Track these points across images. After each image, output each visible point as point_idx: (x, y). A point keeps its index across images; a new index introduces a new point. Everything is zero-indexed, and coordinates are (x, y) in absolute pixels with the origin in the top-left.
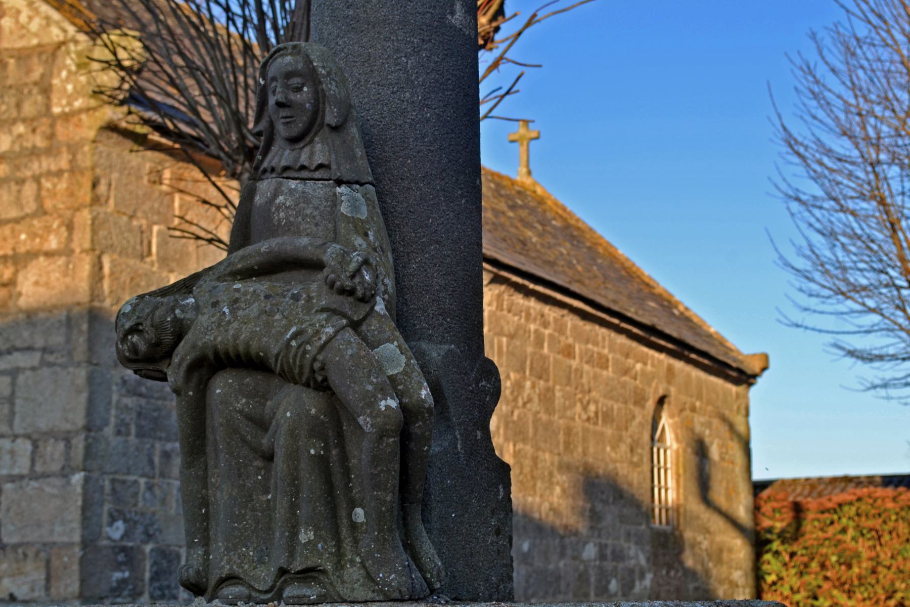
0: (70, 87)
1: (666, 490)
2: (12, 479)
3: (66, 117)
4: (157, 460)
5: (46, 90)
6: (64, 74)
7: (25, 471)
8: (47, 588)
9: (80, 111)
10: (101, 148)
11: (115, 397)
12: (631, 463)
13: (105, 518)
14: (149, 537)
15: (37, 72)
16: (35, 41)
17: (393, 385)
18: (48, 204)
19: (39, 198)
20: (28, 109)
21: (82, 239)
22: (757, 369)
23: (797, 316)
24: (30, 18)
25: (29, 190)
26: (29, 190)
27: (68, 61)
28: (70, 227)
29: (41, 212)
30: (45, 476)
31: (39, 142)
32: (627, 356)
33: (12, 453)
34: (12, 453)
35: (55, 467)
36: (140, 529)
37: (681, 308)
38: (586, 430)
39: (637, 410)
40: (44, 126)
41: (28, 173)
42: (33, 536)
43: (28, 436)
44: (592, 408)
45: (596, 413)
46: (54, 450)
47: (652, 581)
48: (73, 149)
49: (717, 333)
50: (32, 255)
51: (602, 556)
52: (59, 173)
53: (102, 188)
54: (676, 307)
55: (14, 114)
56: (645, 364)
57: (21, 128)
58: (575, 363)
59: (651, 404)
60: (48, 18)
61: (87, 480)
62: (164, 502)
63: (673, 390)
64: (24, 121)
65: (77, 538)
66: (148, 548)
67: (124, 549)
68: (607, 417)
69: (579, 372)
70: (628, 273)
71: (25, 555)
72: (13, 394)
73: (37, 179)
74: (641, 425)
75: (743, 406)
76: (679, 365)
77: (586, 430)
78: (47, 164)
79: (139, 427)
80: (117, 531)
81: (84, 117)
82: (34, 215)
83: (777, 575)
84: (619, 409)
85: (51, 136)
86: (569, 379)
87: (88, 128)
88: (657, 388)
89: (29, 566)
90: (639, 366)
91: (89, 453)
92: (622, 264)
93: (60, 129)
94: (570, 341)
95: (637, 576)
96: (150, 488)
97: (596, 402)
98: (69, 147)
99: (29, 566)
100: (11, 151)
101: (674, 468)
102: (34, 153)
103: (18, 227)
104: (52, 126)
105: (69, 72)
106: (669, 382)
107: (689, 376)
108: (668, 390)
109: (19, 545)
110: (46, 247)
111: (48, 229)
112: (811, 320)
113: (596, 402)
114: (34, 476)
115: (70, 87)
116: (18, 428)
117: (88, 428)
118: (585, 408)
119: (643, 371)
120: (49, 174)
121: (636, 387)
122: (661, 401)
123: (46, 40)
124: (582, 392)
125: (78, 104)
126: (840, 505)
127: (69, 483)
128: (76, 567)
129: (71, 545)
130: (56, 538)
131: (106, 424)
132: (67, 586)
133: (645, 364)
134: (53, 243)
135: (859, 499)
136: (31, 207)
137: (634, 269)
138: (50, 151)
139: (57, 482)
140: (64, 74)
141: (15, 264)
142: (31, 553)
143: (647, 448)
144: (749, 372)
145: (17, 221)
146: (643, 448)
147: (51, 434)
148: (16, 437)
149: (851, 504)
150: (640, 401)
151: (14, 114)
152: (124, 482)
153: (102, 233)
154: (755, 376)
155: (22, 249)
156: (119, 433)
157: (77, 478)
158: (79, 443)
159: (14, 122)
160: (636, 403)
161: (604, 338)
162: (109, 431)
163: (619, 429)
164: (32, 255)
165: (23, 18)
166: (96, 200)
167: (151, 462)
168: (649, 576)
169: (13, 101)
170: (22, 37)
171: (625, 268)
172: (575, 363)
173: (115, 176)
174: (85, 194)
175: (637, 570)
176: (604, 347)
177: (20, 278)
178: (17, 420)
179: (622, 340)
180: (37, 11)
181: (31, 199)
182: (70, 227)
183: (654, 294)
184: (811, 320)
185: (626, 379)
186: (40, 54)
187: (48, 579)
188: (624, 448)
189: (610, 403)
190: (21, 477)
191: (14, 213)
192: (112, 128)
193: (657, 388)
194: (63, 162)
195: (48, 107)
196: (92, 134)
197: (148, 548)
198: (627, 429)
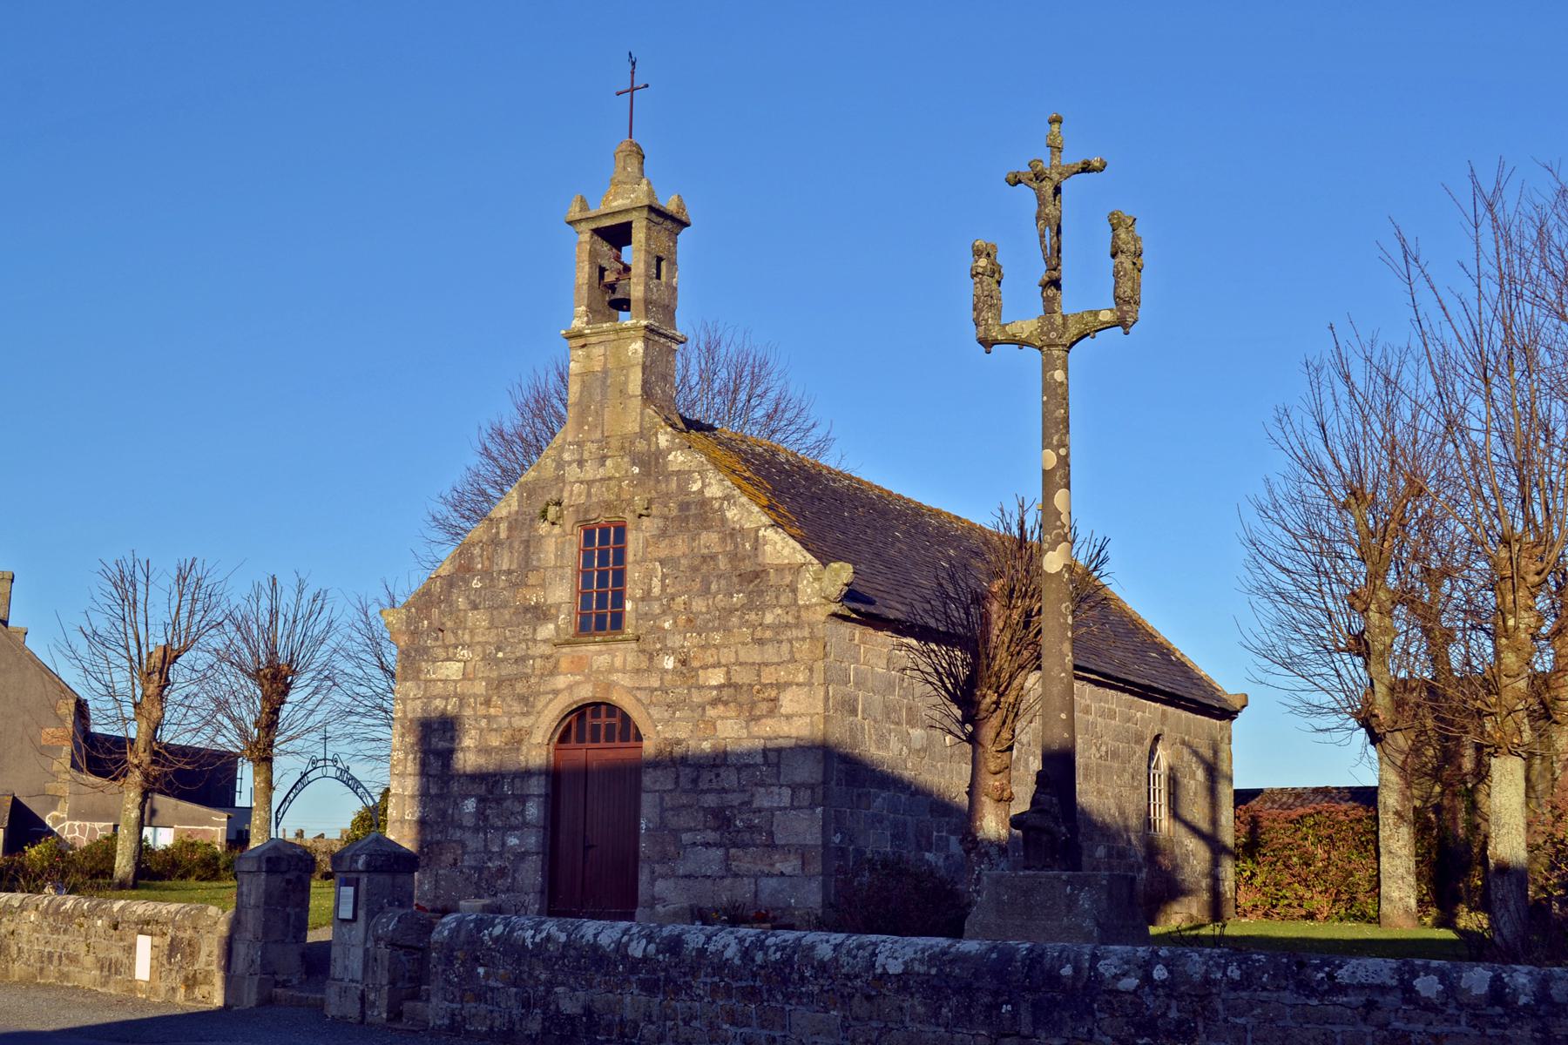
0: (809, 590)
1: (1160, 806)
2: (780, 809)
3: (807, 607)
4: (854, 798)
5: (794, 591)
6: (805, 582)
7: (788, 805)
8: (803, 869)
9: (816, 605)
10: (828, 625)
11: (836, 765)
12: (1132, 786)
13: (832, 832)
14: (852, 842)
15: (788, 579)
16: (786, 561)
17: (1064, 835)
18: (797, 656)
19: (791, 652)
20: (783, 600)
21: (818, 677)
22: (1238, 708)
23: (1261, 676)
24: (783, 547)
25: (785, 647)
26: (785, 647)
27: (808, 575)
28: (811, 670)
29: (793, 660)
30: (800, 808)
31: (791, 620)
32: (1130, 708)
33: (780, 794)
34: (780, 794)
35: (806, 803)
36: (848, 837)
37: (1178, 655)
38: (1099, 765)
39: (1137, 748)
40: (793, 610)
41: (785, 638)
42: (794, 840)
43: (789, 786)
44: (1104, 748)
45: (1107, 752)
46: (805, 795)
47: (1147, 873)
48: (811, 625)
49: (1206, 676)
50: (788, 684)
51: (1109, 855)
52: (804, 639)
53: (828, 648)
54: (1174, 654)
55: (775, 602)
56: (1144, 712)
57: (779, 611)
58: (1091, 718)
59: (1148, 743)
60: (794, 548)
61: (824, 811)
62: (858, 822)
63: (1165, 729)
64: (781, 607)
65: (820, 843)
66: (851, 848)
67: (841, 848)
68: (1115, 754)
69: (1094, 724)
70: (1134, 625)
71: (789, 851)
72: (779, 761)
73: (790, 642)
74: (1141, 758)
75: (1227, 735)
76: (1170, 709)
77: (1099, 765)
78: (795, 633)
79: (846, 781)
80: (837, 839)
81: (818, 608)
82: (789, 662)
83: (1251, 872)
84: (1123, 748)
85: (798, 617)
86: (1087, 730)
87: (820, 614)
88: (1153, 729)
89: (792, 857)
90: (1139, 714)
91: (825, 797)
92: (1131, 616)
93: (803, 614)
94: (1088, 702)
95: (180, 872)
96: (851, 814)
97: (1107, 744)
98: (809, 624)
99: (792, 857)
100: (773, 623)
101: (1167, 788)
102: (787, 625)
103: (779, 668)
104: (798, 611)
105: (808, 581)
106: (1163, 724)
107: (1179, 717)
108: (1162, 730)
109: (786, 846)
110: (796, 680)
111: (798, 670)
112: (1271, 679)
113: (1107, 744)
114: (793, 807)
115: (809, 590)
116: (782, 780)
117: (824, 783)
118: (1098, 750)
119: (1142, 717)
120: (797, 639)
121: (1137, 730)
122: (1157, 738)
123: (793, 561)
124: (1097, 738)
125: (814, 600)
126: (1302, 817)
127: (814, 812)
128: (820, 858)
129: (816, 846)
130: (807, 842)
131: (832, 780)
132: (814, 868)
133: (1144, 712)
134: (801, 678)
135: (1319, 813)
136: (786, 657)
137: (1140, 621)
138: (797, 626)
139: (809, 812)
140: (805, 582)
141: (778, 688)
142: (793, 851)
143: (1145, 775)
144: (1231, 709)
145: (778, 664)
146: (1141, 776)
147: (803, 785)
148: (781, 786)
149: (1311, 815)
150: (1139, 740)
151: (775, 602)
152: (840, 811)
153: (829, 673)
154: (1236, 712)
155: (782, 681)
156: (838, 784)
157: (819, 810)
158: (820, 791)
159: (775, 606)
160: (1136, 742)
161: (1112, 696)
162: (833, 783)
163: (1123, 762)
164: (788, 684)
165: (779, 547)
166: (826, 655)
167: (852, 800)
168: (1145, 870)
169: (774, 594)
170: (779, 558)
171: (1132, 620)
172: (1091, 718)
173: (834, 639)
174: (819, 652)
175: (1136, 866)
176: (1112, 704)
177: (781, 697)
178: (782, 777)
179: (1126, 696)
180: (787, 545)
181: (787, 652)
182: (811, 670)
183: (1156, 643)
184: (1271, 679)
185: (1129, 724)
186: (790, 569)
187: (803, 864)
188: (1127, 776)
189: (1117, 744)
190: (786, 808)
191: (776, 660)
192: (835, 615)
193: (1153, 729)
194: (806, 633)
195: (796, 600)
196: (823, 618)
197: (851, 848)
198: (1129, 762)
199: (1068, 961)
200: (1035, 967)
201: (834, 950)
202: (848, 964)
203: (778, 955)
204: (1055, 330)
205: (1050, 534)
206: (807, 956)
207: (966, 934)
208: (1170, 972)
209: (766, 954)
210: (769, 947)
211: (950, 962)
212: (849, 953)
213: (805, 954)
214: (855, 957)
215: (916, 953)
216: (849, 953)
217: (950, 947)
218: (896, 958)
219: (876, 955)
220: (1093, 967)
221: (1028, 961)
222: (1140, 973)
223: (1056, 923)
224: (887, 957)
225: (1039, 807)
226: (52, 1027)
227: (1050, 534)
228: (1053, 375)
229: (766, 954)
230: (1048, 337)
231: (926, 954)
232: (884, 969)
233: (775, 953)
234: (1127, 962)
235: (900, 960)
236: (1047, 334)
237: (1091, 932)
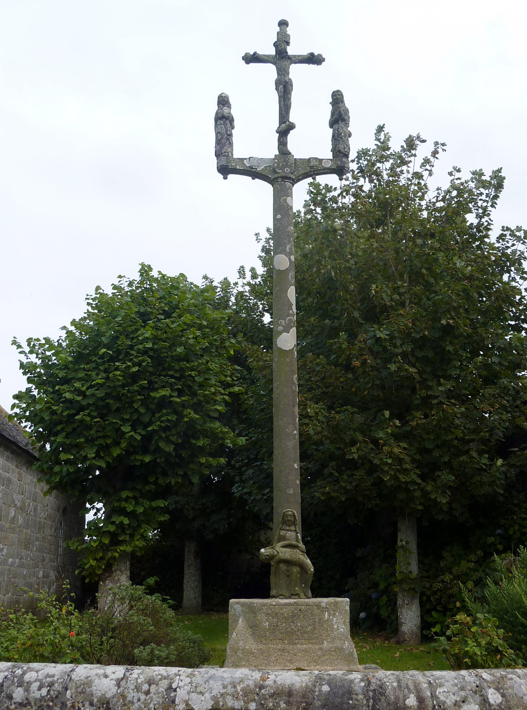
199: (410, 692)
200: (380, 700)
201: (118, 685)
202: (139, 700)
203: (44, 691)
204: (289, 167)
205: (285, 319)
206: (82, 692)
207: (229, 661)
208: (503, 695)
209: (27, 690)
210: (29, 683)
211: (272, 695)
212: (138, 688)
213: (79, 690)
214: (147, 693)
215: (225, 687)
216: (138, 688)
217: (263, 679)
218: (202, 693)
219: (175, 690)
220: (433, 696)
221: (371, 694)
222: (478, 698)
223: (317, 647)
224: (189, 693)
225: (286, 542)
226: (266, 183)
227: (285, 319)
228: (286, 200)
229: (27, 690)
230: (283, 171)
231: (239, 688)
232: (187, 704)
233: (39, 689)
234: (462, 689)
235: (207, 695)
236: (282, 168)
237: (351, 654)
